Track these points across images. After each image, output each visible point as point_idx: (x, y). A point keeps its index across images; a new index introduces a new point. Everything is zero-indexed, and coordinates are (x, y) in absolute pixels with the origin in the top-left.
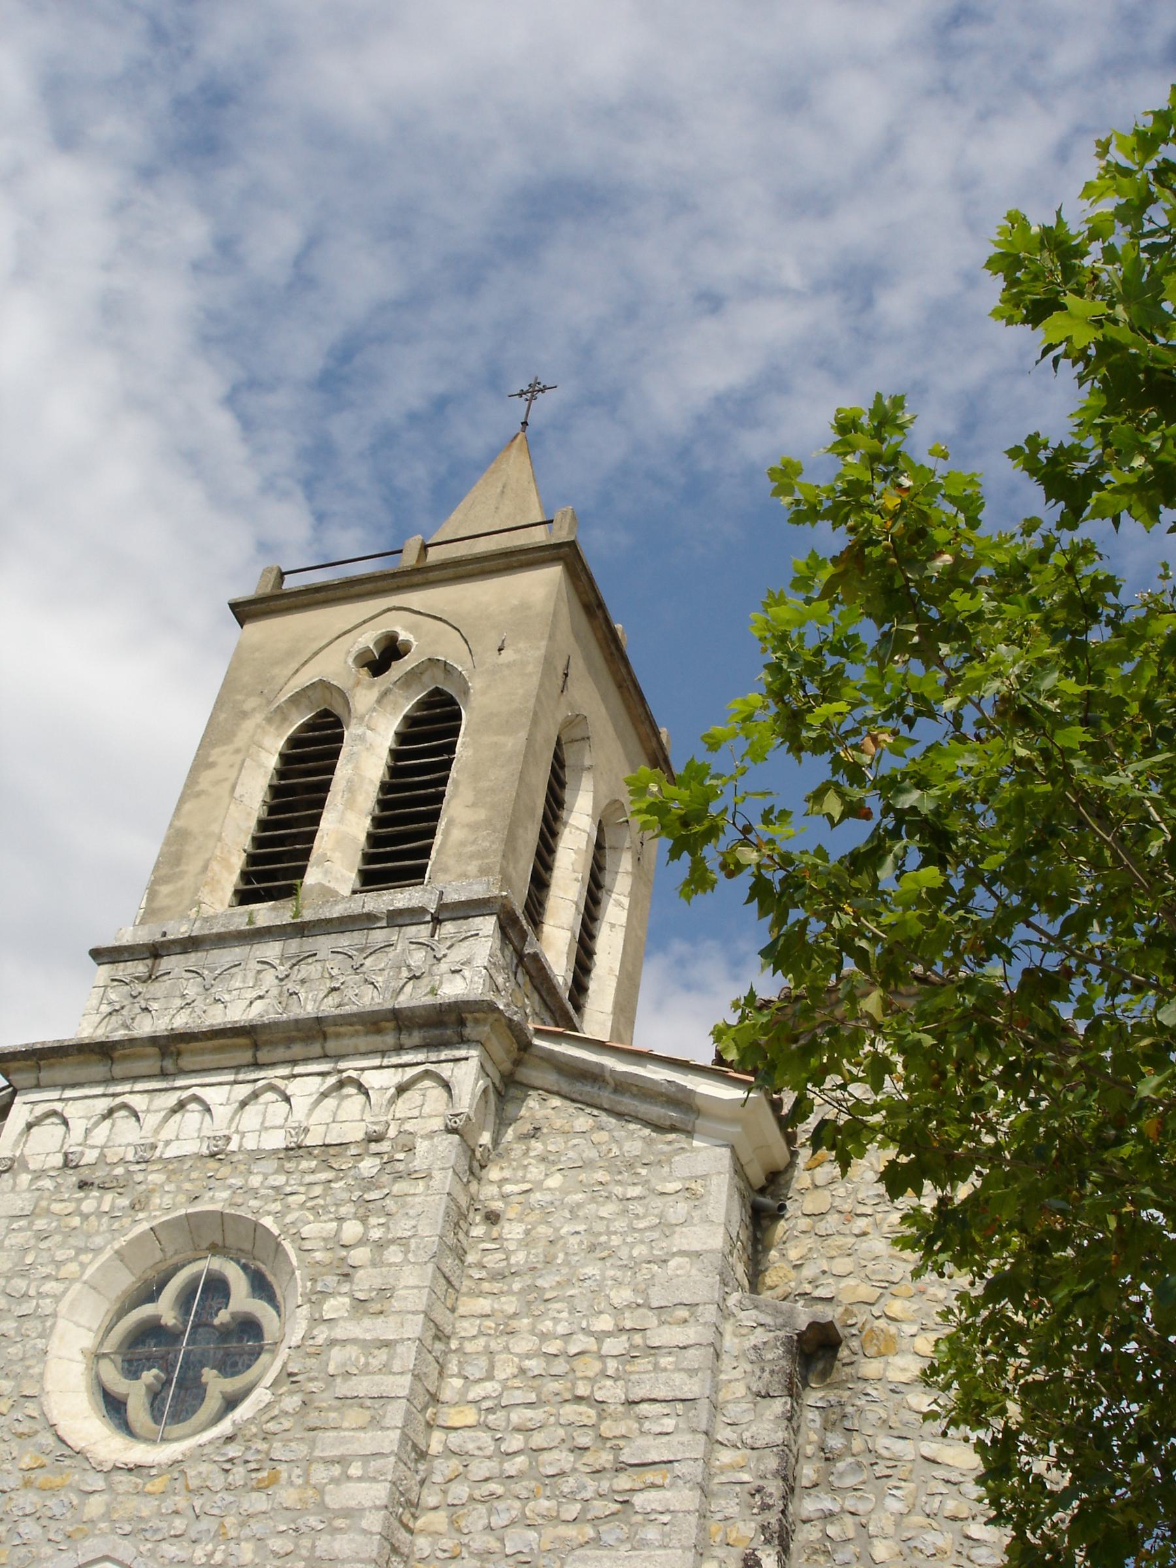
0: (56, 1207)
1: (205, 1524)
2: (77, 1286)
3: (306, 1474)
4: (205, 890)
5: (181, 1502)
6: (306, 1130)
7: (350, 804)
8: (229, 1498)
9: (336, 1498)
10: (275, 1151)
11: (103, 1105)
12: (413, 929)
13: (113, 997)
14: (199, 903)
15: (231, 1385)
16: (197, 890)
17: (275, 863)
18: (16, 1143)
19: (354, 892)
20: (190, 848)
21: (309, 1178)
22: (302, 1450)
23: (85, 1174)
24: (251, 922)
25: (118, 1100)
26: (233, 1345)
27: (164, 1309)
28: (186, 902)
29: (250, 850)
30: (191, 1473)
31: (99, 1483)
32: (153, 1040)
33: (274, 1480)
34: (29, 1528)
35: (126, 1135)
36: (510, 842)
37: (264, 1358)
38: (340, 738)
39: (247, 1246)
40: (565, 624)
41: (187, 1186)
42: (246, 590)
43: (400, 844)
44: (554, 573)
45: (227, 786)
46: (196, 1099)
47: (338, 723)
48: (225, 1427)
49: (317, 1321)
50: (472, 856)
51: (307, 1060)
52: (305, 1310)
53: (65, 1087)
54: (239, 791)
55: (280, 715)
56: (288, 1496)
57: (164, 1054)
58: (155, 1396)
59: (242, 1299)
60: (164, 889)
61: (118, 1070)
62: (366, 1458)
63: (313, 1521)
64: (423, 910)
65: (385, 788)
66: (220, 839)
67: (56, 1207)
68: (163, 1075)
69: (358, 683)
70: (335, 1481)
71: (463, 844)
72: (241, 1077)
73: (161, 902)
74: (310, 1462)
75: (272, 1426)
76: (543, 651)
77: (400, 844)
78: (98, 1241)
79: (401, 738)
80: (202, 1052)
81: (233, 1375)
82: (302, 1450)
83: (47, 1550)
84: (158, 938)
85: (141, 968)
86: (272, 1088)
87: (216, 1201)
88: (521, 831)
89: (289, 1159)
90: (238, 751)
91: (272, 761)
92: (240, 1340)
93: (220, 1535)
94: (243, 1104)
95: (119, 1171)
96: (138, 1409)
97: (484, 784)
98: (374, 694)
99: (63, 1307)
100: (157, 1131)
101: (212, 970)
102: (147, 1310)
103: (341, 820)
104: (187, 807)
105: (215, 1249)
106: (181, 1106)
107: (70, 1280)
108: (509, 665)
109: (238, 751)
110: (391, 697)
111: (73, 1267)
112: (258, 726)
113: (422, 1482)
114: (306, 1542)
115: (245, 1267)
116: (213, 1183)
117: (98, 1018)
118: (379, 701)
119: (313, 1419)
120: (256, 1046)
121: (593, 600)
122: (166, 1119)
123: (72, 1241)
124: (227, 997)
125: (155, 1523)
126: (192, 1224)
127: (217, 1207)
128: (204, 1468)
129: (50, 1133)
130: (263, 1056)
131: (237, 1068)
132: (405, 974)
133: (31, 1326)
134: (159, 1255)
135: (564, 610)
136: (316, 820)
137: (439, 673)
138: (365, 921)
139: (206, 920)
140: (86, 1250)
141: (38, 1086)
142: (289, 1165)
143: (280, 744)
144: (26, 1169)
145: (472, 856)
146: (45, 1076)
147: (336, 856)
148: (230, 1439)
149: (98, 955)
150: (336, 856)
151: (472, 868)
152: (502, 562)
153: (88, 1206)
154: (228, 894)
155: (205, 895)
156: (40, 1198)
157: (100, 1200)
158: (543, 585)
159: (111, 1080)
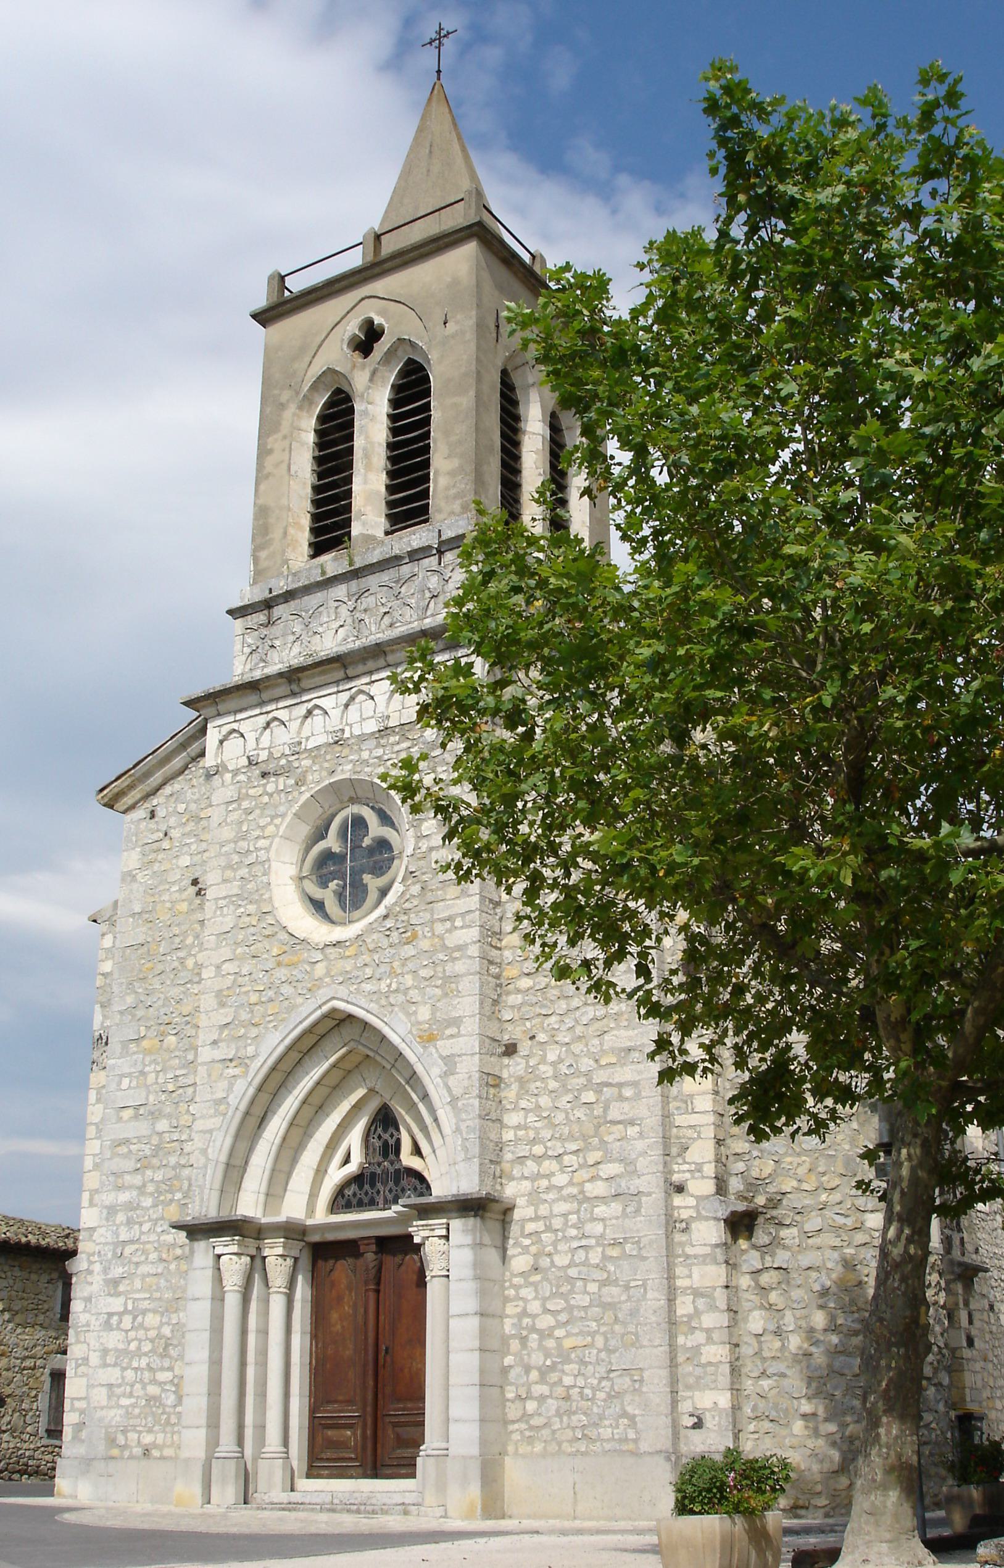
0: (252, 792)
1: (383, 968)
2: (277, 840)
3: (432, 930)
4: (289, 550)
5: (366, 958)
6: (388, 717)
7: (368, 467)
8: (393, 951)
9: (451, 941)
10: (373, 733)
11: (262, 720)
12: (427, 560)
13: (250, 641)
14: (286, 562)
15: (381, 881)
16: (284, 551)
17: (330, 526)
18: (216, 755)
19: (387, 533)
20: (272, 520)
21: (396, 748)
22: (427, 916)
23: (264, 767)
24: (323, 573)
25: (271, 716)
26: (377, 857)
27: (332, 842)
28: (279, 562)
29: (312, 510)
30: (368, 941)
31: (319, 956)
32: (281, 675)
33: (415, 936)
34: (286, 990)
35: (282, 737)
36: (479, 481)
37: (396, 862)
38: (352, 410)
39: (371, 796)
40: (488, 286)
41: (326, 765)
42: (261, 301)
43: (408, 502)
44: (470, 249)
45: (284, 466)
46: (317, 707)
47: (348, 399)
48: (381, 910)
49: (420, 837)
50: (455, 497)
51: (378, 670)
52: (411, 832)
53: (236, 712)
54: (293, 468)
55: (307, 401)
56: (425, 944)
57: (290, 681)
58: (340, 896)
59: (376, 829)
60: (263, 554)
61: (265, 696)
62: (463, 915)
63: (441, 956)
64: (430, 547)
65: (391, 446)
66: (289, 509)
67: (252, 792)
68: (294, 694)
69: (354, 366)
70: (448, 931)
71: (447, 488)
72: (341, 688)
73: (263, 564)
74: (433, 922)
75: (407, 905)
76: (474, 320)
77: (408, 502)
78: (282, 809)
79: (395, 403)
80: (313, 676)
81: (382, 874)
82: (427, 916)
83: (300, 1000)
84: (267, 595)
85: (261, 617)
86: (361, 692)
87: (345, 772)
88: (485, 467)
89: (382, 737)
90: (285, 437)
91: (311, 438)
92: (381, 853)
93: (393, 973)
94: (347, 706)
95: (283, 762)
96: (332, 906)
97: (454, 438)
98: (366, 374)
99: (272, 854)
100: (299, 733)
101: (307, 612)
102: (322, 845)
103: (365, 482)
104: (262, 487)
105: (353, 800)
106: (309, 713)
107: (273, 837)
108: (453, 336)
109: (285, 437)
110: (379, 374)
111: (271, 829)
112: (294, 415)
113: (501, 919)
114: (440, 969)
115: (373, 808)
116: (341, 761)
117: (244, 658)
118: (371, 380)
119: (430, 896)
120: (345, 667)
121: (505, 254)
122: (303, 723)
123: (267, 812)
124: (320, 630)
125: (356, 973)
126: (335, 788)
127: (346, 776)
128: (375, 936)
129: (234, 743)
130: (351, 672)
131: (337, 682)
132: (428, 595)
133: (255, 869)
134: (320, 810)
135: (486, 275)
136: (349, 480)
137: (409, 349)
138: (394, 561)
139: (295, 575)
140: (277, 816)
141: (219, 715)
142: (382, 741)
143: (313, 422)
144: (228, 771)
145: (455, 497)
146: (222, 708)
147: (368, 509)
148: (386, 917)
149: (233, 613)
150: (368, 509)
151: (457, 506)
152: (433, 246)
153: (270, 788)
154: (305, 549)
155: (290, 554)
156: (240, 788)
157: (276, 782)
158: (464, 259)
159: (263, 703)
